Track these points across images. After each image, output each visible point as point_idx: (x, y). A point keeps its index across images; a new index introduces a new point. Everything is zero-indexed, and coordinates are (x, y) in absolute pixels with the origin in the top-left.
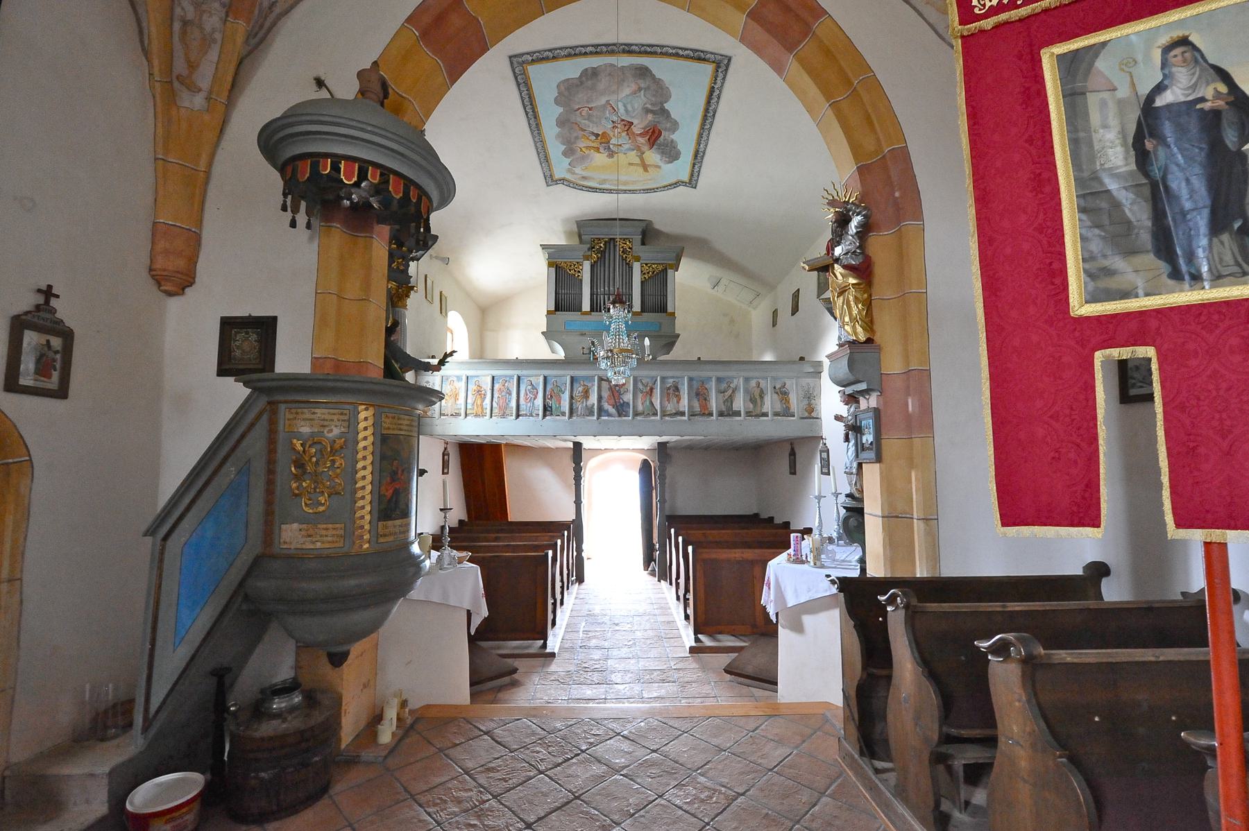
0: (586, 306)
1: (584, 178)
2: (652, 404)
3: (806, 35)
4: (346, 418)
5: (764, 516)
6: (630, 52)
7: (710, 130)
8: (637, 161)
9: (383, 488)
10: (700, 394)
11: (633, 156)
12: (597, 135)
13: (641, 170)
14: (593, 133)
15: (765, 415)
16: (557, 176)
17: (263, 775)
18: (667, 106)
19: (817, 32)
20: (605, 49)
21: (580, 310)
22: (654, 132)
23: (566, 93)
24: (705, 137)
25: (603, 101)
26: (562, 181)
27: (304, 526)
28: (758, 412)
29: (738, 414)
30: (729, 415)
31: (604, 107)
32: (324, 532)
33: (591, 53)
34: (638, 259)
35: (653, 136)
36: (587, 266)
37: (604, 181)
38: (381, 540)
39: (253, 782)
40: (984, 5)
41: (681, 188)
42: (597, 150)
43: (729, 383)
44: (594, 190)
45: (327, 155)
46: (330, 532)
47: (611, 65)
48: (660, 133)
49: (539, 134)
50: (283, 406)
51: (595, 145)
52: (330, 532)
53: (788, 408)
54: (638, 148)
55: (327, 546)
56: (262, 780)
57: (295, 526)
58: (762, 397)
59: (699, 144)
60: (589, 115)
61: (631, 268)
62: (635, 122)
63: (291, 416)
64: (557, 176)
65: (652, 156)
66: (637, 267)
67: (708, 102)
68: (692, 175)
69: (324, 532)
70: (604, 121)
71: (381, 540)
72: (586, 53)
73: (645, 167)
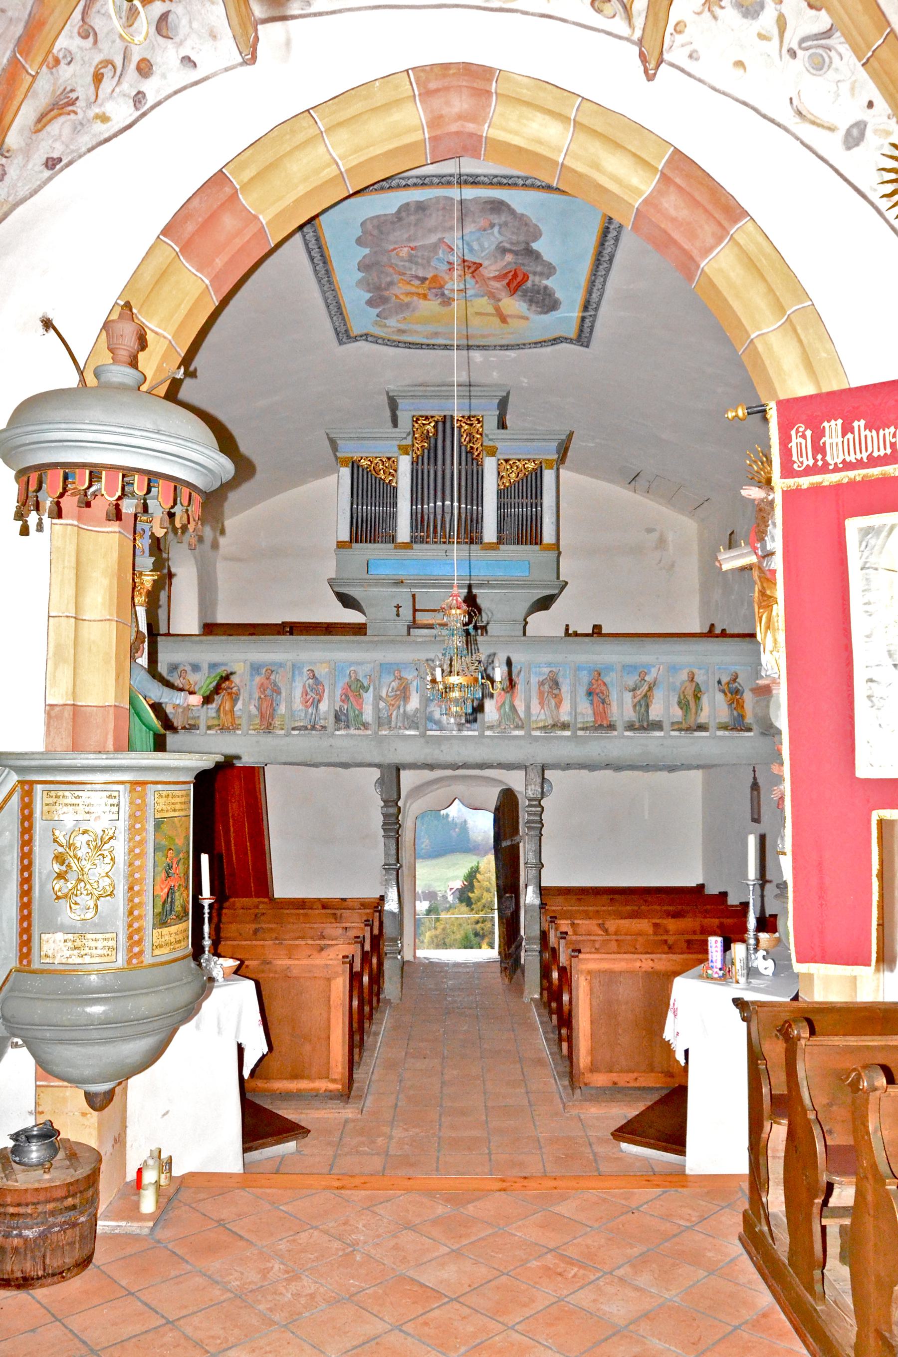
0: (404, 532)
1: (402, 331)
2: (513, 708)
3: (720, 240)
4: (115, 801)
5: (712, 889)
6: (475, 183)
7: (606, 276)
8: (490, 309)
9: (157, 887)
10: (596, 693)
11: (483, 304)
12: (423, 280)
13: (497, 320)
14: (417, 277)
15: (701, 728)
16: (356, 331)
17: (26, 1233)
18: (535, 246)
19: (736, 236)
20: (436, 180)
21: (393, 539)
22: (515, 276)
23: (375, 232)
24: (598, 285)
25: (433, 238)
26: (366, 337)
27: (70, 936)
28: (691, 722)
29: (657, 726)
30: (642, 728)
31: (435, 247)
32: (93, 944)
33: (415, 185)
34: (492, 452)
35: (515, 282)
36: (405, 464)
37: (436, 334)
38: (157, 952)
39: (16, 1241)
40: (802, 463)
41: (564, 345)
42: (425, 297)
43: (642, 676)
44: (420, 346)
45: (84, 465)
46: (100, 944)
47: (446, 198)
48: (526, 278)
49: (330, 282)
50: (39, 787)
51: (421, 291)
52: (100, 944)
53: (742, 717)
54: (492, 296)
55: (98, 960)
56: (26, 1240)
57: (60, 936)
58: (697, 698)
59: (590, 292)
60: (411, 256)
61: (480, 465)
62: (486, 263)
63: (50, 801)
64: (356, 331)
65: (514, 305)
66: (490, 465)
67: (602, 243)
68: (581, 331)
69: (93, 944)
70: (433, 263)
71: (157, 952)
72: (407, 186)
73: (503, 319)
